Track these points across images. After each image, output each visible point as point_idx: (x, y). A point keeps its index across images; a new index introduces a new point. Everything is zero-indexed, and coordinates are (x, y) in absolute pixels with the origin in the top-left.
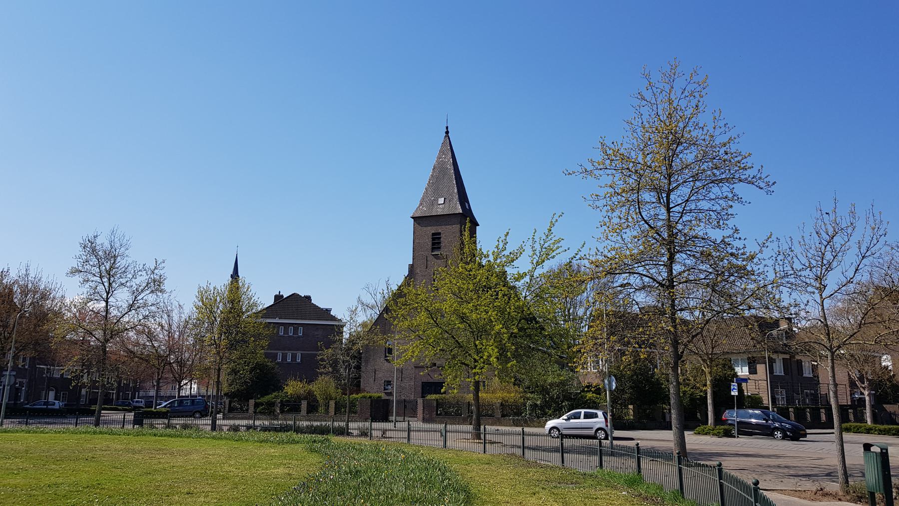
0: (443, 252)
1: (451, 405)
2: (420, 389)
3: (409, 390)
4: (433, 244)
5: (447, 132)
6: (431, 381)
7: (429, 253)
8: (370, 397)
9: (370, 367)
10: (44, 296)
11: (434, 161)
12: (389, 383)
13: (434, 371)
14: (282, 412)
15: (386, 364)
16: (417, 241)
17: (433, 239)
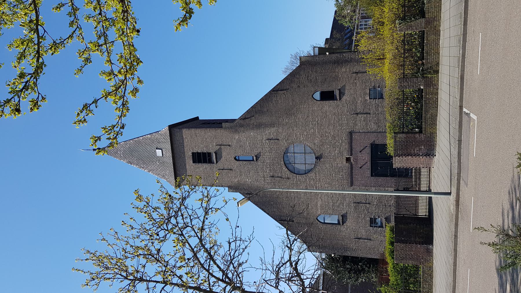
0: (212, 149)
2: (381, 179)
3: (385, 194)
4: (205, 162)
6: (369, 164)
8: (392, 243)
9: (353, 246)
10: (504, 233)
11: (124, 162)
13: (356, 160)
15: (348, 223)
17: (199, 162)
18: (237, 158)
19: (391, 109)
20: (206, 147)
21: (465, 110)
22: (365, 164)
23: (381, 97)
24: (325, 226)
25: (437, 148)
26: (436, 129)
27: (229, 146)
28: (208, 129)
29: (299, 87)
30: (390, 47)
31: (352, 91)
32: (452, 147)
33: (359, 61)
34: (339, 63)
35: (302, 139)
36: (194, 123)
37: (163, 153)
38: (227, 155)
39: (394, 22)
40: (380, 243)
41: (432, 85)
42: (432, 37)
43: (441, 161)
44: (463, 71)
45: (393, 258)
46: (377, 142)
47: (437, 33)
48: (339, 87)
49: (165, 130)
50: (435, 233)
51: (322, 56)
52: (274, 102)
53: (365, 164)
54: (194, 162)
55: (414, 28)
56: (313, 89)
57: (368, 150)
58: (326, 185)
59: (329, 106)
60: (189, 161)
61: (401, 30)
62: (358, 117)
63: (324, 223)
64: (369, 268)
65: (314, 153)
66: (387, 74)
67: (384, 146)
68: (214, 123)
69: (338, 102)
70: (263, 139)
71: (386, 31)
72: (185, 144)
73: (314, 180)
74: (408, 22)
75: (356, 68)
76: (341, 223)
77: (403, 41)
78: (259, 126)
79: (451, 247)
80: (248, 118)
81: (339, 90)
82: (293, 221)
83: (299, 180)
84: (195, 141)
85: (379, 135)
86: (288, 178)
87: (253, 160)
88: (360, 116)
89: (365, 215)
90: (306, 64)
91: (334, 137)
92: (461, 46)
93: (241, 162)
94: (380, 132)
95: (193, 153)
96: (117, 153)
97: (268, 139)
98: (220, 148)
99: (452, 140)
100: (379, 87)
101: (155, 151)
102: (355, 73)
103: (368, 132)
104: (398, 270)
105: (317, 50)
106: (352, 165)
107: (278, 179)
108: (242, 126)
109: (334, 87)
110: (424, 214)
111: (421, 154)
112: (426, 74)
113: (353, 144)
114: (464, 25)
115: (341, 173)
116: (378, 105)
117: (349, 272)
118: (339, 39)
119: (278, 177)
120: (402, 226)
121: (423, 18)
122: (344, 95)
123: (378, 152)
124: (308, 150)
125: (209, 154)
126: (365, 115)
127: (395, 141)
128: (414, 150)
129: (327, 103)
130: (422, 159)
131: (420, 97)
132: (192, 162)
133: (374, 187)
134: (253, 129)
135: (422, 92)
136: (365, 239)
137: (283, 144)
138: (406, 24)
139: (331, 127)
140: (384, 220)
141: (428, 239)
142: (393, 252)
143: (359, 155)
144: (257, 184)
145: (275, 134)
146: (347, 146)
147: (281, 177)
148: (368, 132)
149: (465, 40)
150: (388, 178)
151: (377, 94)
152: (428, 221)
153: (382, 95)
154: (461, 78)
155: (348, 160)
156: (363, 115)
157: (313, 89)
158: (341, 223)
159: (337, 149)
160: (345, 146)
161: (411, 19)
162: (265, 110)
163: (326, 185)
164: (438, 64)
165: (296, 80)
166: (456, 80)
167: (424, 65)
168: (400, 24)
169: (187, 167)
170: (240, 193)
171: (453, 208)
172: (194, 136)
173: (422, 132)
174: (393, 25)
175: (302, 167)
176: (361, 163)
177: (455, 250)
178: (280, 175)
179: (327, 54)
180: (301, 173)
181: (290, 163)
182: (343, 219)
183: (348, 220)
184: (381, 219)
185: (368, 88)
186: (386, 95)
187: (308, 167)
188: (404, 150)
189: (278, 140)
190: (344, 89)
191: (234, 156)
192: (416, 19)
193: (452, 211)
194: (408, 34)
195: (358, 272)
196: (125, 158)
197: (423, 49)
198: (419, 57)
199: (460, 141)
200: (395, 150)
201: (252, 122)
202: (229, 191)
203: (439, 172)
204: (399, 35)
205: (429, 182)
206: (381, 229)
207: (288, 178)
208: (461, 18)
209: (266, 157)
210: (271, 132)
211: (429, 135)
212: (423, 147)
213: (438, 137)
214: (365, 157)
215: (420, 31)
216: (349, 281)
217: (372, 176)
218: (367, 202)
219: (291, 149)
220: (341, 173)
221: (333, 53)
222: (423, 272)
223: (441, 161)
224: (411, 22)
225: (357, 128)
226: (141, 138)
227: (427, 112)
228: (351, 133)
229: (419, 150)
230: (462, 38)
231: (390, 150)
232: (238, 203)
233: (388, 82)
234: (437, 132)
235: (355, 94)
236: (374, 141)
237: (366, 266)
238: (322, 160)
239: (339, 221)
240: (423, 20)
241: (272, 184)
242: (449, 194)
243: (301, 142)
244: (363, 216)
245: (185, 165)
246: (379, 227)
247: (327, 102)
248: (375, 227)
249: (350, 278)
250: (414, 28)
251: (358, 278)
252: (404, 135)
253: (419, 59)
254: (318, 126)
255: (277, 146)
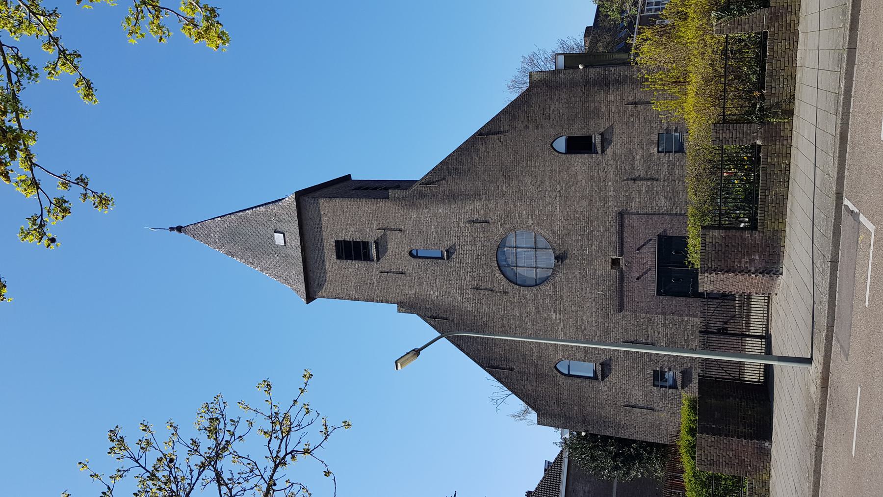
0: (370, 236)
1: (724, 189)
2: (675, 301)
4: (358, 257)
5: (179, 229)
6: (654, 272)
7: (375, 267)
8: (692, 432)
11: (220, 253)
12: (658, 377)
13: (630, 264)
14: (734, 296)
15: (614, 377)
16: (353, 292)
18: (414, 253)
19: (697, 179)
20: (361, 231)
21: (846, 202)
22: (646, 273)
23: (681, 149)
24: (569, 381)
25: (786, 261)
26: (784, 223)
27: (400, 230)
28: (364, 200)
29: (527, 127)
30: (698, 61)
31: (625, 138)
32: (816, 270)
33: (639, 83)
34: (600, 84)
35: (531, 222)
36: (344, 187)
37: (285, 239)
38: (396, 247)
39: (706, 14)
40: (673, 416)
41: (780, 138)
42: (783, 45)
43: (793, 290)
44: (845, 122)
45: (693, 458)
46: (670, 233)
47: (793, 38)
48: (602, 130)
49: (290, 199)
50: (775, 420)
51: (570, 71)
52: (481, 155)
53: (646, 273)
54: (338, 257)
55: (747, 27)
56: (552, 132)
57: (653, 247)
58: (573, 308)
59: (583, 164)
60: (330, 256)
61: (720, 32)
62: (635, 186)
63: (569, 375)
64: (650, 453)
65: (553, 249)
66: (692, 112)
67: (682, 241)
68: (376, 189)
69: (600, 157)
70: (460, 220)
71: (690, 32)
72: (324, 225)
73: (551, 297)
74: (735, 15)
75: (635, 95)
76: (600, 377)
77: (725, 52)
78: (454, 197)
79: (808, 463)
80: (434, 182)
81: (602, 134)
82: (512, 369)
83: (525, 297)
84: (341, 220)
85: (675, 220)
86: (505, 292)
87: (442, 258)
88: (639, 183)
89: (645, 364)
90: (541, 87)
91: (589, 221)
92: (844, 71)
93: (421, 260)
94: (676, 214)
95: (337, 242)
96: (208, 236)
97: (469, 221)
98: (385, 235)
99: (818, 259)
100: (676, 131)
101: (273, 236)
102: (633, 103)
103: (654, 214)
104: (702, 481)
105: (561, 59)
106: (621, 272)
107: (486, 292)
108: (422, 196)
109: (593, 130)
110: (755, 378)
111: (753, 270)
112: (768, 116)
113: (625, 235)
114: (850, 30)
115: (602, 287)
116: (675, 164)
117: (614, 459)
118: (609, 30)
119: (486, 289)
120: (713, 401)
121: (765, 7)
122: (610, 143)
123: (671, 249)
124: (542, 242)
125: (366, 245)
126: (649, 183)
127: (704, 243)
128: (740, 262)
129: (578, 158)
130: (756, 279)
131: (755, 161)
132: (334, 256)
133: (662, 314)
134: (442, 201)
135: (759, 151)
136: (643, 408)
137: (497, 231)
138: (730, 19)
139: (585, 203)
140: (679, 376)
141: (762, 429)
142: (694, 446)
143: (636, 254)
144: (448, 300)
145: (482, 212)
146: (613, 239)
147: (492, 290)
148: (654, 214)
149: (851, 61)
150: (689, 300)
151: (672, 142)
152: (762, 393)
153: (682, 145)
154: (841, 138)
155: (615, 263)
156: (645, 182)
157: (552, 132)
158: (600, 377)
159: (595, 243)
160: (611, 238)
161: (741, 9)
162: (465, 168)
163: (573, 308)
164: (792, 99)
165: (522, 115)
166: (830, 139)
167: (764, 99)
168: (719, 19)
169: (327, 265)
170: (419, 315)
171: (814, 390)
172: (339, 212)
173: (756, 228)
174: (704, 21)
175: (530, 274)
176: (638, 270)
177: (817, 473)
178: (489, 286)
179: (581, 67)
180: (528, 283)
181: (509, 266)
182: (602, 370)
183: (613, 372)
184: (674, 374)
185: (656, 132)
186: (690, 143)
187: (541, 274)
188: (723, 260)
189: (488, 222)
190: (611, 133)
191: (408, 250)
192: (751, 10)
193: (814, 396)
194: (733, 38)
195: (629, 460)
196: (221, 245)
197: (763, 69)
198: (754, 83)
199: (834, 262)
200: (703, 260)
201: (441, 190)
202: (399, 311)
203: (788, 308)
204: (715, 39)
205: (768, 319)
206: (674, 391)
207: (505, 292)
208: (844, 13)
209: (466, 254)
210: (475, 208)
211: (769, 234)
212: (757, 257)
213: (787, 241)
214: (647, 260)
215: (759, 33)
216: (614, 476)
217: (659, 293)
218: (649, 341)
219: (511, 241)
220: (602, 287)
221: (592, 66)
222: (751, 490)
223: (793, 290)
224: (741, 14)
225: (634, 206)
226: (249, 212)
227: (766, 189)
228: (621, 215)
229: (750, 264)
230: (845, 56)
231: (694, 257)
232: (396, 362)
233: (693, 129)
234: (787, 229)
235: (632, 143)
236: (665, 231)
237: (645, 450)
238: (567, 261)
239: (595, 372)
240: (765, 11)
241: (476, 301)
242: (809, 361)
243: (528, 228)
244: (640, 366)
245: (323, 261)
246: (670, 387)
247: (579, 156)
248: (662, 386)
249: (616, 468)
250: (747, 27)
251: (629, 469)
252: (722, 233)
253: (756, 90)
254: (560, 200)
255: (486, 235)
